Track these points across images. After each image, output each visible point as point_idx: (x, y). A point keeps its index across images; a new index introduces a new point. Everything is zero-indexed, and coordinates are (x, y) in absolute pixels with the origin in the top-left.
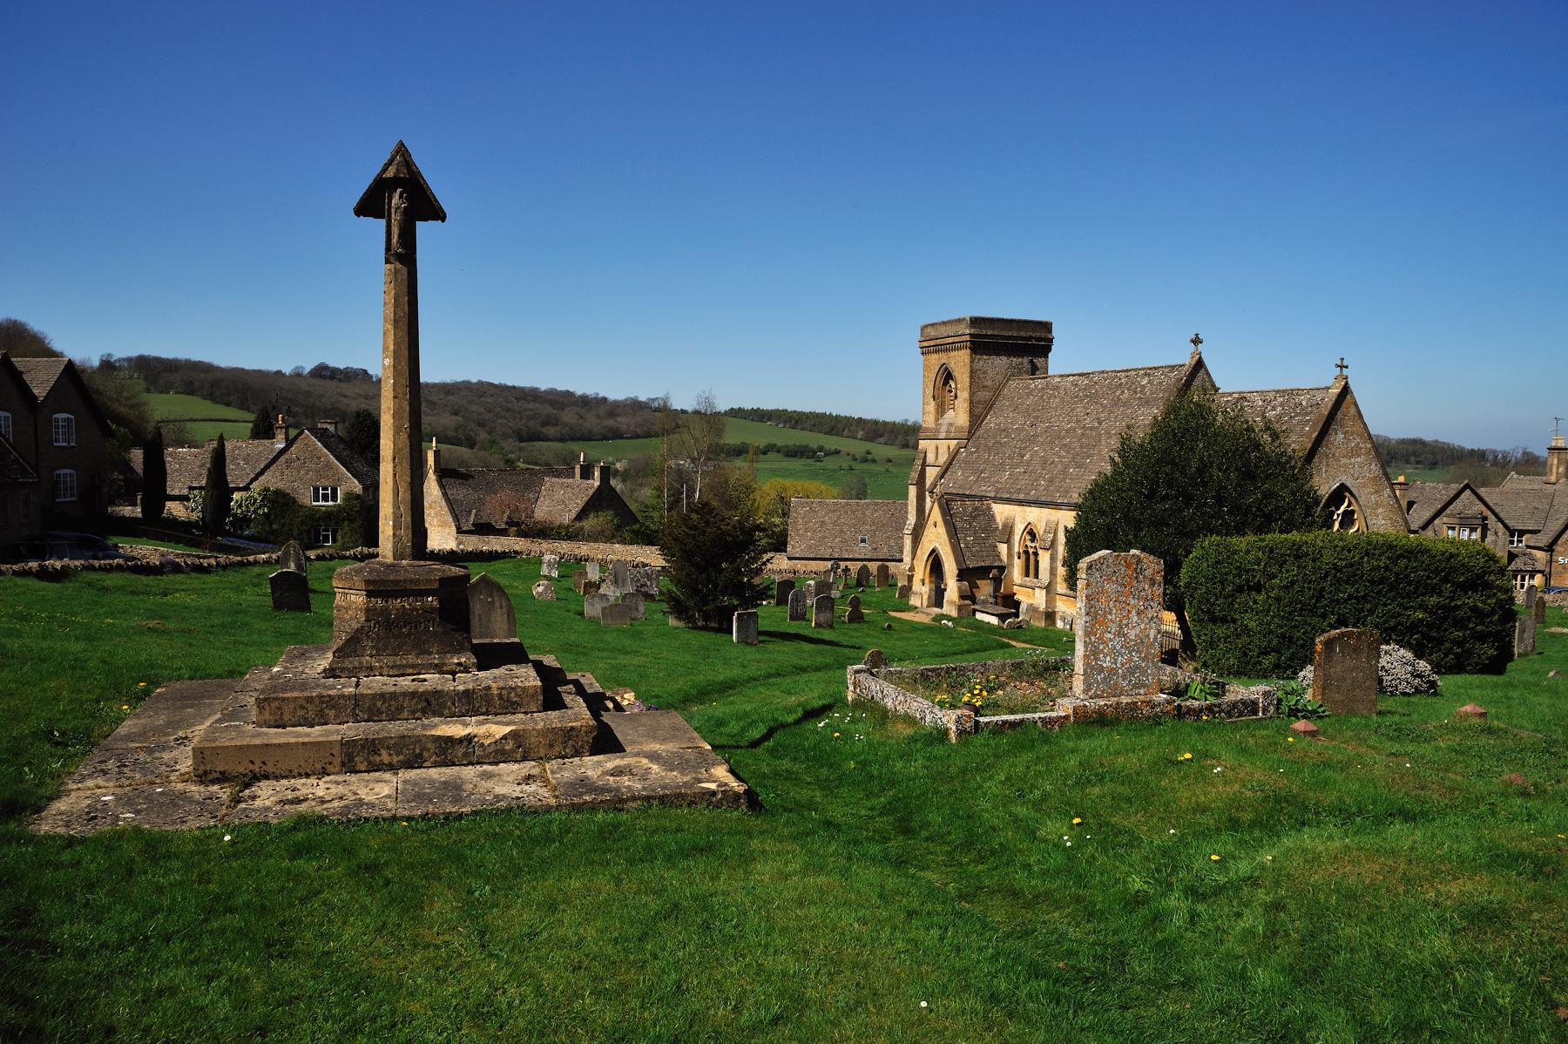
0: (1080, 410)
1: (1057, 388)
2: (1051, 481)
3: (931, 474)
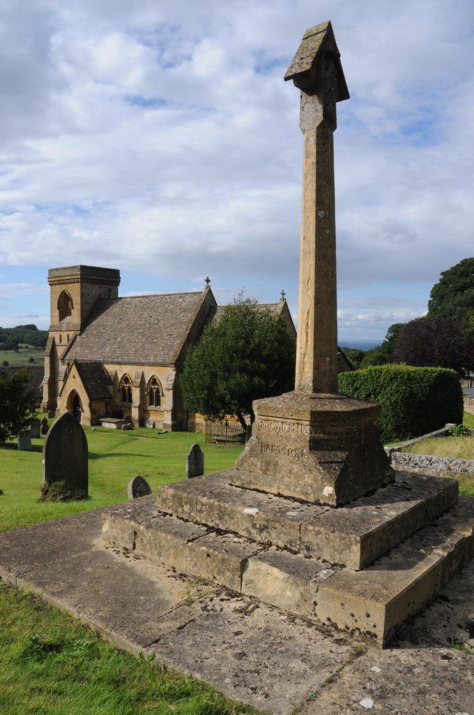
0: (146, 315)
1: (129, 304)
2: (136, 351)
3: (60, 351)
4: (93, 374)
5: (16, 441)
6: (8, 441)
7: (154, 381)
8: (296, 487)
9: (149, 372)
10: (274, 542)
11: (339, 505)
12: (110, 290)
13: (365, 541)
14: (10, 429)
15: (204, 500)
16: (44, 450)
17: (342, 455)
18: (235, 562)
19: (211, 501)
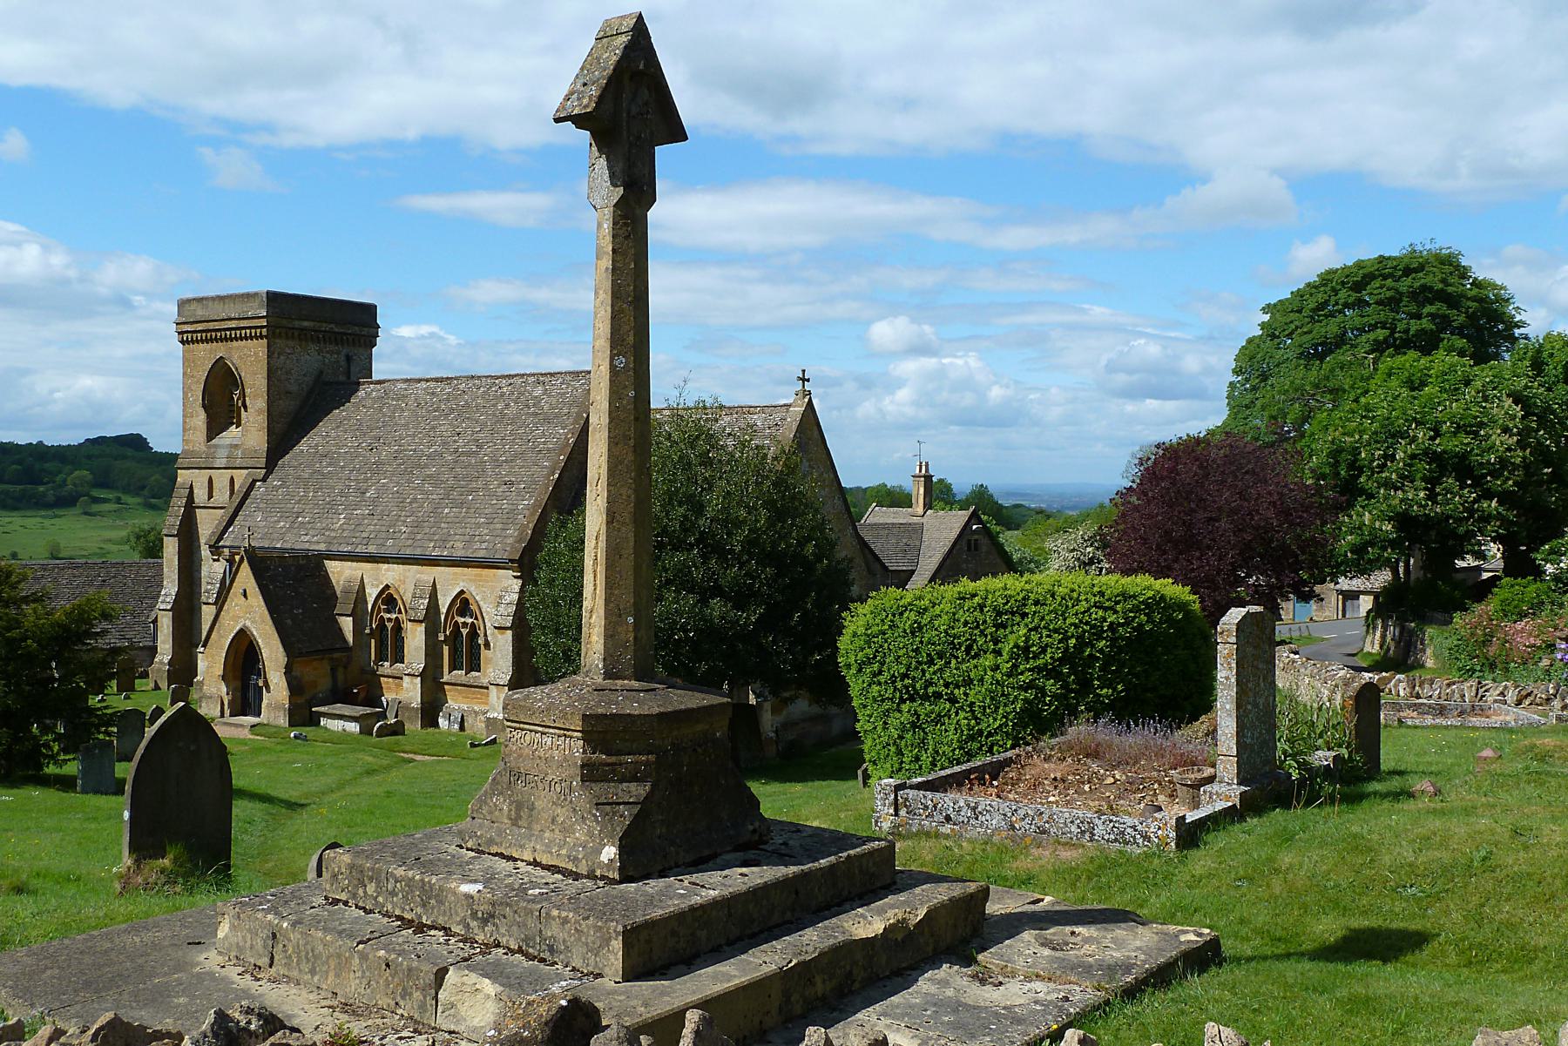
0: (444, 428)
2: (418, 525)
4: (294, 584)
5: (72, 768)
6: (51, 769)
7: (463, 604)
8: (561, 847)
9: (451, 583)
10: (504, 941)
11: (626, 878)
12: (348, 359)
13: (631, 936)
14: (59, 738)
15: (400, 872)
16: (128, 788)
17: (639, 790)
18: (428, 971)
19: (410, 873)
